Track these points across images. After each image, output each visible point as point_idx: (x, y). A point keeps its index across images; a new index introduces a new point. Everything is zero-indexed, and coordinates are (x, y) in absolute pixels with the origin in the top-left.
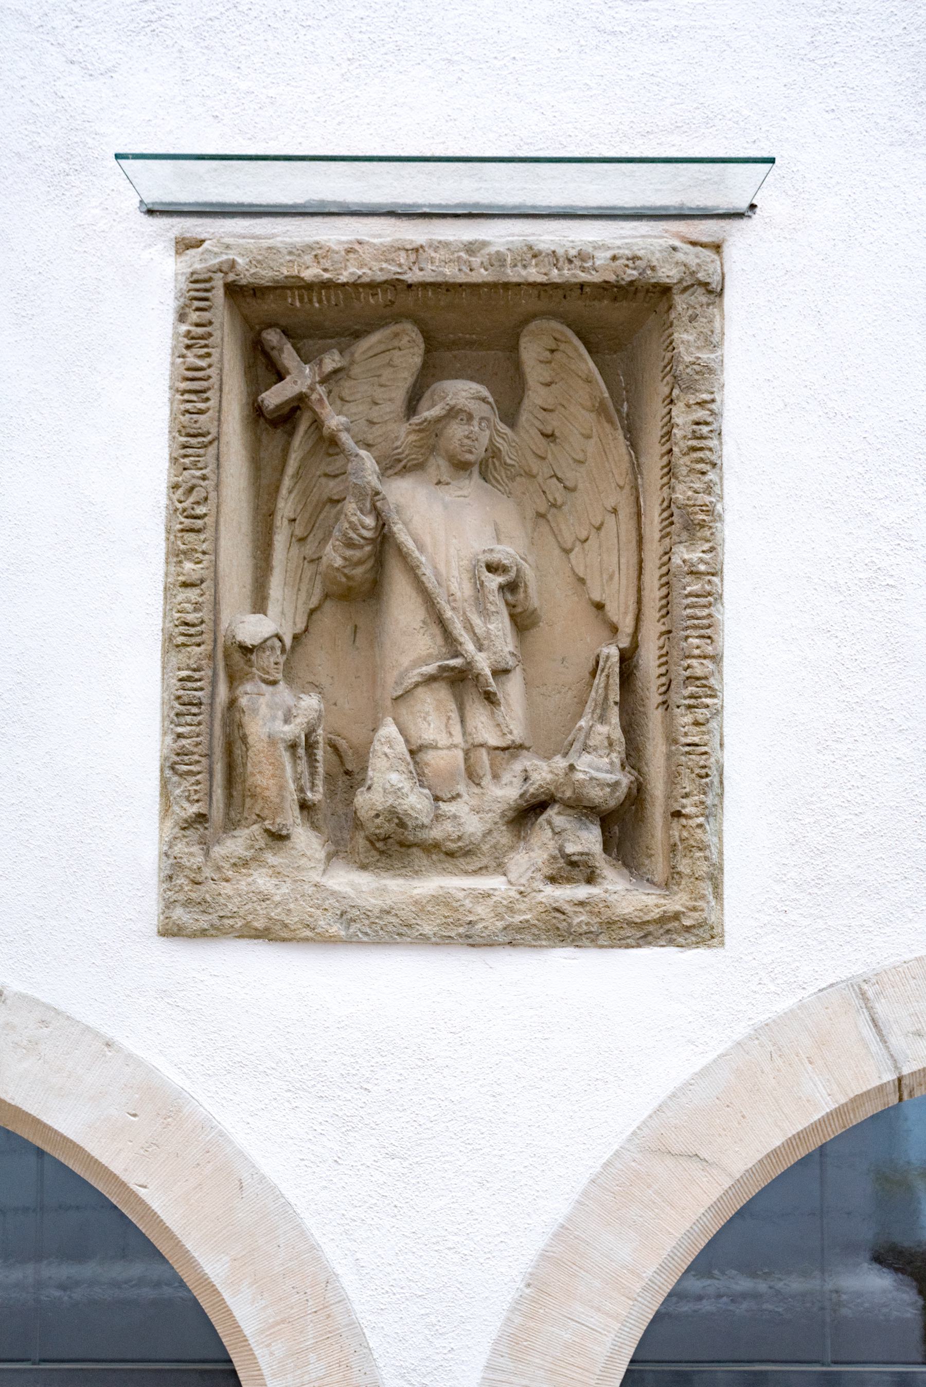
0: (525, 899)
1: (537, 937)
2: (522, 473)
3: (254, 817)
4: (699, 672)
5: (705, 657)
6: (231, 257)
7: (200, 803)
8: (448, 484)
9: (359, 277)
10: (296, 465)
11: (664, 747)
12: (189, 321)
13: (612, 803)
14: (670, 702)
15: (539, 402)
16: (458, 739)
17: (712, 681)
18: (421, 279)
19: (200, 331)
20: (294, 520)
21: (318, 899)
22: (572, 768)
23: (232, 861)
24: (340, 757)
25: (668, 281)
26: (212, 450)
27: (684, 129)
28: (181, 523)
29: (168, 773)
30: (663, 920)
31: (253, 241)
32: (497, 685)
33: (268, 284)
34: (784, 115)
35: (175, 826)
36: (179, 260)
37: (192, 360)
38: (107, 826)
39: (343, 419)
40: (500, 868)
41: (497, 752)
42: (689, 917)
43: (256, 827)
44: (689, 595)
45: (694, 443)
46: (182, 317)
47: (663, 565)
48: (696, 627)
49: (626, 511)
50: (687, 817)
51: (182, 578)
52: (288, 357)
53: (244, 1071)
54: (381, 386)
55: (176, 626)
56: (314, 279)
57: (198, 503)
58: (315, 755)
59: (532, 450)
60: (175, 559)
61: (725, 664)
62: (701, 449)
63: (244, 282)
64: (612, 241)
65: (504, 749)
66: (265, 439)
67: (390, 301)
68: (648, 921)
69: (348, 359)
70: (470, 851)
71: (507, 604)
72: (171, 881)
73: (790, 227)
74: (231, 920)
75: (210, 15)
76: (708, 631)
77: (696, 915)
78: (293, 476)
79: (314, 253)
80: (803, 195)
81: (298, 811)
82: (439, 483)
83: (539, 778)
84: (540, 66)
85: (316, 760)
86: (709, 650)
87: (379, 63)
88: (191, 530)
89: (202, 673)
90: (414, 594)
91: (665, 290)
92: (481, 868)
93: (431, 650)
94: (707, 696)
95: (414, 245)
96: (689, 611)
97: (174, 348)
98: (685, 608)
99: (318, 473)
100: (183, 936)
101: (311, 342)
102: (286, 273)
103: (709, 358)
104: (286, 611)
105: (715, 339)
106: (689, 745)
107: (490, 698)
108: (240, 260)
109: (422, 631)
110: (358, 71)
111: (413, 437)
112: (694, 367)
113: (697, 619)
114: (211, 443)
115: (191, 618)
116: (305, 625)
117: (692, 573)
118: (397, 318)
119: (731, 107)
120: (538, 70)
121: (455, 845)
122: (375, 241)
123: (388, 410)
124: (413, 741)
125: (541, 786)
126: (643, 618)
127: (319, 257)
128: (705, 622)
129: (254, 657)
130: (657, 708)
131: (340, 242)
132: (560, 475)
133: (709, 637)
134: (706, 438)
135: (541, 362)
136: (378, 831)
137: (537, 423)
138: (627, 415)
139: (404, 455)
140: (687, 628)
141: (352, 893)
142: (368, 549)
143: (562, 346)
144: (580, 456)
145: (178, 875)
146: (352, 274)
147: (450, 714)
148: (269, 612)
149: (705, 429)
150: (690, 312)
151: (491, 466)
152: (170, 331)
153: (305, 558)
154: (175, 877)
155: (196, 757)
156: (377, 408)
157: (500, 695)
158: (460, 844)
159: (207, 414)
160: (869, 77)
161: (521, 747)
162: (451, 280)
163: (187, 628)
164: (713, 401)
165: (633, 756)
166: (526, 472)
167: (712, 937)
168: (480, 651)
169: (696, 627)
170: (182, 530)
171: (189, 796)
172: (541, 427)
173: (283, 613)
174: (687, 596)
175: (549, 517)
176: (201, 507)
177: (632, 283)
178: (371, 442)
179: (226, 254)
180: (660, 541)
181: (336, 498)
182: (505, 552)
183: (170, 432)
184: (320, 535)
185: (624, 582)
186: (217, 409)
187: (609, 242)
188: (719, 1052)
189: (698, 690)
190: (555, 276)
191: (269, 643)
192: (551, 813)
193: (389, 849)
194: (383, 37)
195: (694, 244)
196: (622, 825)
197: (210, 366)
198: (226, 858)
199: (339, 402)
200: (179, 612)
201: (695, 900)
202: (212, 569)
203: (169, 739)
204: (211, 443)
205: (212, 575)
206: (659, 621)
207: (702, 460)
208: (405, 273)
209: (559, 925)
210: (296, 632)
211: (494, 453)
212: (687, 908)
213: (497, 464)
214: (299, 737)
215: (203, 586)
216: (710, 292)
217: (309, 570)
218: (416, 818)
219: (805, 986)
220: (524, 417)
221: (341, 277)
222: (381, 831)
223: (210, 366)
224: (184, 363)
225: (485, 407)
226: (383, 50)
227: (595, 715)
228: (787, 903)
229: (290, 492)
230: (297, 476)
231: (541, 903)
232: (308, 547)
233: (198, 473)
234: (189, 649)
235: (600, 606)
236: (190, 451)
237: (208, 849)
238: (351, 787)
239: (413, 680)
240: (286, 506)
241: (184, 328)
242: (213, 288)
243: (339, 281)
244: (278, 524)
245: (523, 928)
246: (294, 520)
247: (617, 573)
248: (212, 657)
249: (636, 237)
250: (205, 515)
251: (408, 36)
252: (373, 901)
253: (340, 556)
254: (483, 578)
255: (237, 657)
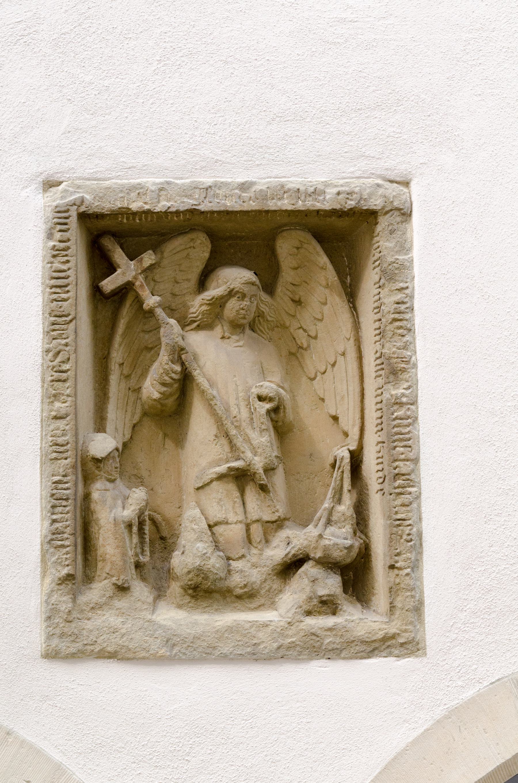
0: (292, 628)
1: (300, 653)
2: (279, 325)
3: (106, 575)
4: (404, 470)
5: (408, 460)
6: (81, 195)
7: (70, 567)
8: (229, 338)
9: (169, 208)
10: (124, 327)
11: (382, 520)
12: (55, 238)
13: (349, 560)
14: (385, 490)
15: (290, 279)
16: (241, 517)
17: (412, 477)
18: (210, 209)
19: (62, 245)
20: (123, 364)
21: (150, 631)
22: (321, 536)
23: (91, 606)
24: (157, 527)
25: (375, 208)
26: (72, 326)
27: (382, 107)
28: (52, 376)
29: (46, 547)
30: (385, 639)
31: (96, 182)
32: (267, 478)
33: (106, 213)
34: (448, 98)
35: (52, 583)
36: (46, 195)
37: (57, 265)
38: (5, 583)
39: (157, 298)
40: (272, 605)
41: (268, 524)
42: (403, 636)
43: (106, 581)
44: (396, 418)
45: (397, 316)
46: (50, 236)
47: (378, 395)
48: (401, 440)
49: (352, 354)
50: (400, 569)
51: (54, 413)
52: (119, 256)
53: (103, 749)
54: (181, 271)
55: (51, 446)
56: (138, 210)
57: (63, 362)
58: (144, 529)
59: (285, 310)
60: (48, 400)
61: (421, 464)
62: (401, 320)
63: (91, 212)
64: (337, 180)
65: (273, 522)
66: (100, 307)
67: (188, 219)
68: (375, 640)
69: (159, 256)
70: (252, 594)
71: (272, 420)
72: (50, 621)
73: (455, 172)
74: (92, 646)
75: (63, 31)
76: (408, 442)
77: (406, 635)
78: (123, 334)
79: (138, 192)
80: (462, 151)
81: (134, 570)
82: (223, 338)
83: (298, 543)
84: (285, 65)
85: (144, 533)
86: (411, 455)
87: (178, 63)
88: (59, 381)
89: (69, 478)
90: (208, 417)
91: (372, 215)
92: (260, 606)
93: (221, 456)
94: (409, 487)
95: (205, 186)
96: (396, 429)
97: (44, 257)
98: (393, 428)
99: (138, 330)
100: (59, 658)
101: (131, 239)
102: (120, 206)
103: (403, 259)
104: (118, 427)
105: (407, 246)
106: (399, 520)
107: (263, 488)
108: (87, 197)
109: (215, 442)
110: (164, 68)
111: (204, 308)
112: (395, 265)
113: (401, 434)
114: (71, 321)
115: (60, 440)
116: (130, 435)
117: (397, 403)
118: (192, 229)
119: (413, 93)
120: (284, 67)
121: (242, 591)
122: (178, 182)
123: (186, 286)
124: (210, 519)
125: (300, 549)
126: (366, 428)
127: (141, 194)
128: (407, 436)
129: (102, 465)
130: (377, 492)
131: (154, 184)
132: (305, 327)
133: (410, 447)
134: (403, 313)
135: (290, 254)
136: (189, 583)
137: (289, 293)
138: (350, 285)
139: (198, 319)
140: (394, 441)
141: (174, 626)
142: (176, 386)
143: (305, 246)
144: (319, 316)
145: (55, 617)
146: (164, 206)
147: (236, 500)
148: (108, 430)
149: (403, 307)
150: (390, 228)
151: (257, 322)
152: (41, 245)
153: (129, 389)
154: (52, 617)
155: (66, 536)
156: (178, 285)
157: (269, 486)
158: (246, 590)
159: (68, 301)
160: (502, 73)
161: (285, 519)
162: (230, 209)
163: (58, 447)
164: (407, 288)
165: (361, 520)
166: (281, 325)
167: (418, 650)
168: (255, 455)
169: (401, 440)
170: (53, 381)
171: (61, 562)
172: (291, 296)
173: (116, 429)
174: (394, 419)
175: (298, 355)
176: (65, 365)
177: (351, 209)
178: (174, 308)
179: (78, 192)
180: (375, 379)
181: (150, 346)
182: (269, 387)
183: (43, 314)
184: (139, 372)
185: (351, 404)
186: (75, 298)
187: (335, 182)
188: (425, 727)
189: (403, 481)
190: (300, 205)
191: (112, 455)
192: (307, 567)
193: (197, 595)
194: (180, 45)
195: (392, 182)
196: (355, 575)
197: (69, 269)
198: (87, 604)
199: (152, 283)
200: (52, 436)
201: (406, 625)
202: (74, 407)
203: (47, 523)
204: (71, 321)
205: (74, 411)
206: (376, 433)
207: (401, 327)
208: (199, 204)
209: (315, 644)
210: (125, 440)
211: (260, 315)
212: (401, 630)
213: (261, 321)
214: (134, 519)
215: (68, 418)
216: (403, 214)
217: (133, 397)
218: (216, 574)
219: (481, 681)
220: (279, 290)
221: (157, 208)
222: (192, 582)
223: (69, 269)
224: (51, 267)
225: (254, 288)
226: (180, 54)
227: (335, 499)
228: (467, 625)
229: (120, 345)
230: (124, 335)
231: (303, 629)
232: (132, 381)
233: (64, 342)
234: (59, 462)
235: (335, 418)
236: (57, 327)
237: (75, 598)
238: (165, 548)
239: (210, 477)
240: (117, 354)
241: (51, 243)
242: (70, 216)
243: (155, 211)
244: (113, 368)
245: (292, 646)
246: (123, 364)
247: (346, 396)
248: (74, 467)
249: (353, 178)
250: (68, 370)
251: (197, 44)
252: (188, 631)
253: (157, 391)
254: (256, 406)
255: (90, 465)
